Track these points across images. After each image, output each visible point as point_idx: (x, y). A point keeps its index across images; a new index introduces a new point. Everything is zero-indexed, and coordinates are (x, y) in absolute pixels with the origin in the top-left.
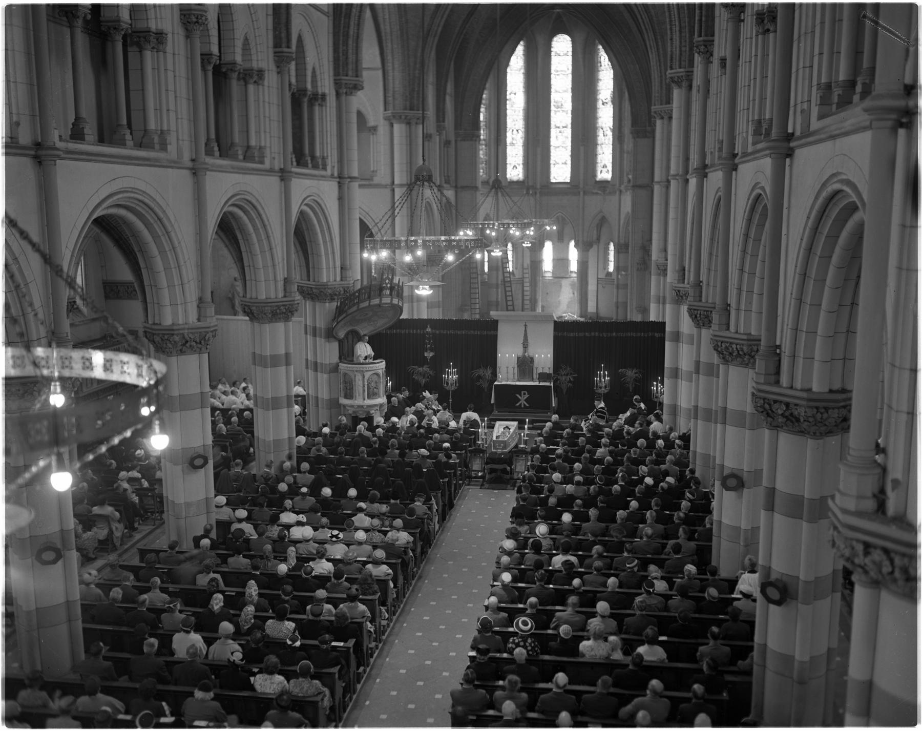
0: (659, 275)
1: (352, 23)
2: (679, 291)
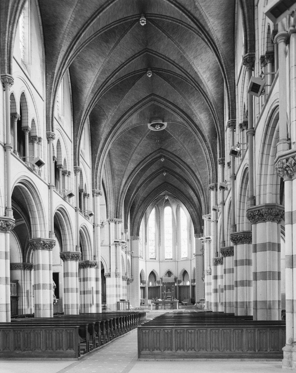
1: (98, 172)
2: (216, 260)
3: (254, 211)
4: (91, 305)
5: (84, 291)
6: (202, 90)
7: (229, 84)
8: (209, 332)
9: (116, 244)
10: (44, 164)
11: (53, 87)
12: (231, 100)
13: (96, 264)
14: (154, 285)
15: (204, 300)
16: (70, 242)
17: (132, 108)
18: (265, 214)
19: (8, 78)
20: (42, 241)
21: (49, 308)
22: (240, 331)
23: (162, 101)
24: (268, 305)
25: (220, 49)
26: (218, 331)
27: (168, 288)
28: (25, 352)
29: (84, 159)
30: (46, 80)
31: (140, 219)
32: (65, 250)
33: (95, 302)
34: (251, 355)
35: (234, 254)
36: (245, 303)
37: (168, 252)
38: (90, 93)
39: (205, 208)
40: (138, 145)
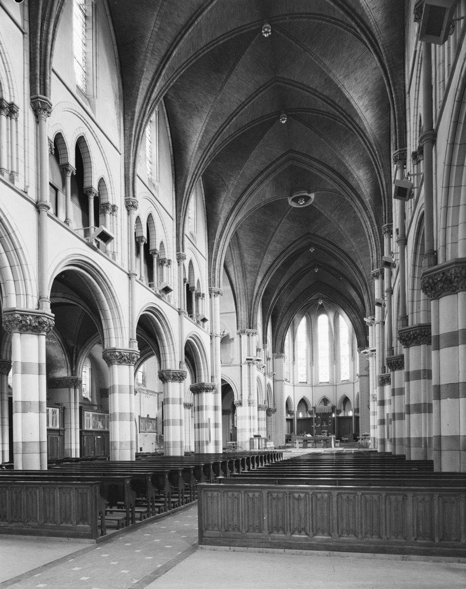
0: (374, 401)
2: (383, 377)
3: (435, 276)
4: (207, 443)
5: (199, 424)
6: (358, 126)
7: (395, 93)
8: (335, 499)
9: (249, 363)
10: (113, 238)
11: (133, 133)
12: (398, 118)
13: (213, 388)
14: (306, 417)
15: (368, 435)
16: (171, 357)
17: (262, 172)
18: (455, 277)
19: (41, 102)
20: (118, 352)
21: (37, 450)
22: (400, 498)
23: (304, 158)
24: (461, 443)
25: (380, 38)
26: (354, 497)
27: (324, 420)
28: (14, 524)
29: (195, 247)
30: (124, 124)
31: (285, 331)
32: (165, 368)
33: (213, 439)
34: (423, 548)
35: (405, 365)
36: (423, 440)
37: (324, 375)
38: (196, 149)
39: (370, 309)
40: (276, 230)
